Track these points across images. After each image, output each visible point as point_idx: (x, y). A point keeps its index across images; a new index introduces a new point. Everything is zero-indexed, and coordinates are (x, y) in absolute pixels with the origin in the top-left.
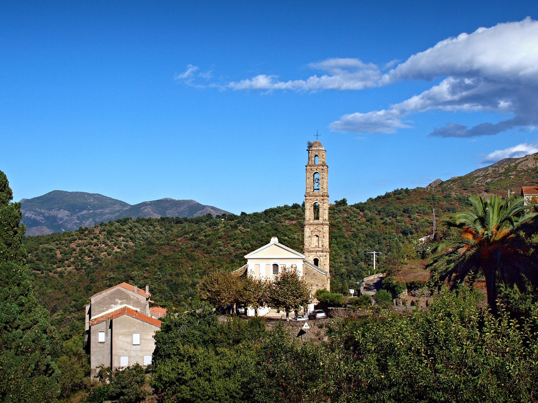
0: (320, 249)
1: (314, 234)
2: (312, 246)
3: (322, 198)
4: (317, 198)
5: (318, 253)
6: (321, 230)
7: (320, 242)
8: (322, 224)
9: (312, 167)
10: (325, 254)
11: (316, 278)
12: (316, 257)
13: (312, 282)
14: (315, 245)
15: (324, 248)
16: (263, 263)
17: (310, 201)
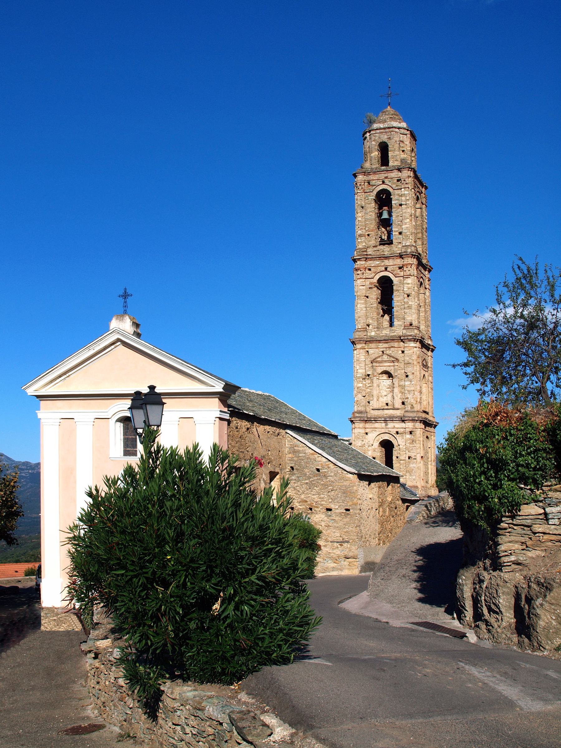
0: (398, 413)
1: (380, 370)
2: (375, 404)
3: (399, 262)
4: (387, 262)
5: (391, 425)
6: (399, 355)
7: (396, 390)
8: (401, 339)
9: (371, 177)
10: (409, 425)
11: (325, 486)
12: (387, 437)
13: (313, 497)
14: (384, 400)
15: (408, 408)
16: (83, 413)
17: (368, 274)
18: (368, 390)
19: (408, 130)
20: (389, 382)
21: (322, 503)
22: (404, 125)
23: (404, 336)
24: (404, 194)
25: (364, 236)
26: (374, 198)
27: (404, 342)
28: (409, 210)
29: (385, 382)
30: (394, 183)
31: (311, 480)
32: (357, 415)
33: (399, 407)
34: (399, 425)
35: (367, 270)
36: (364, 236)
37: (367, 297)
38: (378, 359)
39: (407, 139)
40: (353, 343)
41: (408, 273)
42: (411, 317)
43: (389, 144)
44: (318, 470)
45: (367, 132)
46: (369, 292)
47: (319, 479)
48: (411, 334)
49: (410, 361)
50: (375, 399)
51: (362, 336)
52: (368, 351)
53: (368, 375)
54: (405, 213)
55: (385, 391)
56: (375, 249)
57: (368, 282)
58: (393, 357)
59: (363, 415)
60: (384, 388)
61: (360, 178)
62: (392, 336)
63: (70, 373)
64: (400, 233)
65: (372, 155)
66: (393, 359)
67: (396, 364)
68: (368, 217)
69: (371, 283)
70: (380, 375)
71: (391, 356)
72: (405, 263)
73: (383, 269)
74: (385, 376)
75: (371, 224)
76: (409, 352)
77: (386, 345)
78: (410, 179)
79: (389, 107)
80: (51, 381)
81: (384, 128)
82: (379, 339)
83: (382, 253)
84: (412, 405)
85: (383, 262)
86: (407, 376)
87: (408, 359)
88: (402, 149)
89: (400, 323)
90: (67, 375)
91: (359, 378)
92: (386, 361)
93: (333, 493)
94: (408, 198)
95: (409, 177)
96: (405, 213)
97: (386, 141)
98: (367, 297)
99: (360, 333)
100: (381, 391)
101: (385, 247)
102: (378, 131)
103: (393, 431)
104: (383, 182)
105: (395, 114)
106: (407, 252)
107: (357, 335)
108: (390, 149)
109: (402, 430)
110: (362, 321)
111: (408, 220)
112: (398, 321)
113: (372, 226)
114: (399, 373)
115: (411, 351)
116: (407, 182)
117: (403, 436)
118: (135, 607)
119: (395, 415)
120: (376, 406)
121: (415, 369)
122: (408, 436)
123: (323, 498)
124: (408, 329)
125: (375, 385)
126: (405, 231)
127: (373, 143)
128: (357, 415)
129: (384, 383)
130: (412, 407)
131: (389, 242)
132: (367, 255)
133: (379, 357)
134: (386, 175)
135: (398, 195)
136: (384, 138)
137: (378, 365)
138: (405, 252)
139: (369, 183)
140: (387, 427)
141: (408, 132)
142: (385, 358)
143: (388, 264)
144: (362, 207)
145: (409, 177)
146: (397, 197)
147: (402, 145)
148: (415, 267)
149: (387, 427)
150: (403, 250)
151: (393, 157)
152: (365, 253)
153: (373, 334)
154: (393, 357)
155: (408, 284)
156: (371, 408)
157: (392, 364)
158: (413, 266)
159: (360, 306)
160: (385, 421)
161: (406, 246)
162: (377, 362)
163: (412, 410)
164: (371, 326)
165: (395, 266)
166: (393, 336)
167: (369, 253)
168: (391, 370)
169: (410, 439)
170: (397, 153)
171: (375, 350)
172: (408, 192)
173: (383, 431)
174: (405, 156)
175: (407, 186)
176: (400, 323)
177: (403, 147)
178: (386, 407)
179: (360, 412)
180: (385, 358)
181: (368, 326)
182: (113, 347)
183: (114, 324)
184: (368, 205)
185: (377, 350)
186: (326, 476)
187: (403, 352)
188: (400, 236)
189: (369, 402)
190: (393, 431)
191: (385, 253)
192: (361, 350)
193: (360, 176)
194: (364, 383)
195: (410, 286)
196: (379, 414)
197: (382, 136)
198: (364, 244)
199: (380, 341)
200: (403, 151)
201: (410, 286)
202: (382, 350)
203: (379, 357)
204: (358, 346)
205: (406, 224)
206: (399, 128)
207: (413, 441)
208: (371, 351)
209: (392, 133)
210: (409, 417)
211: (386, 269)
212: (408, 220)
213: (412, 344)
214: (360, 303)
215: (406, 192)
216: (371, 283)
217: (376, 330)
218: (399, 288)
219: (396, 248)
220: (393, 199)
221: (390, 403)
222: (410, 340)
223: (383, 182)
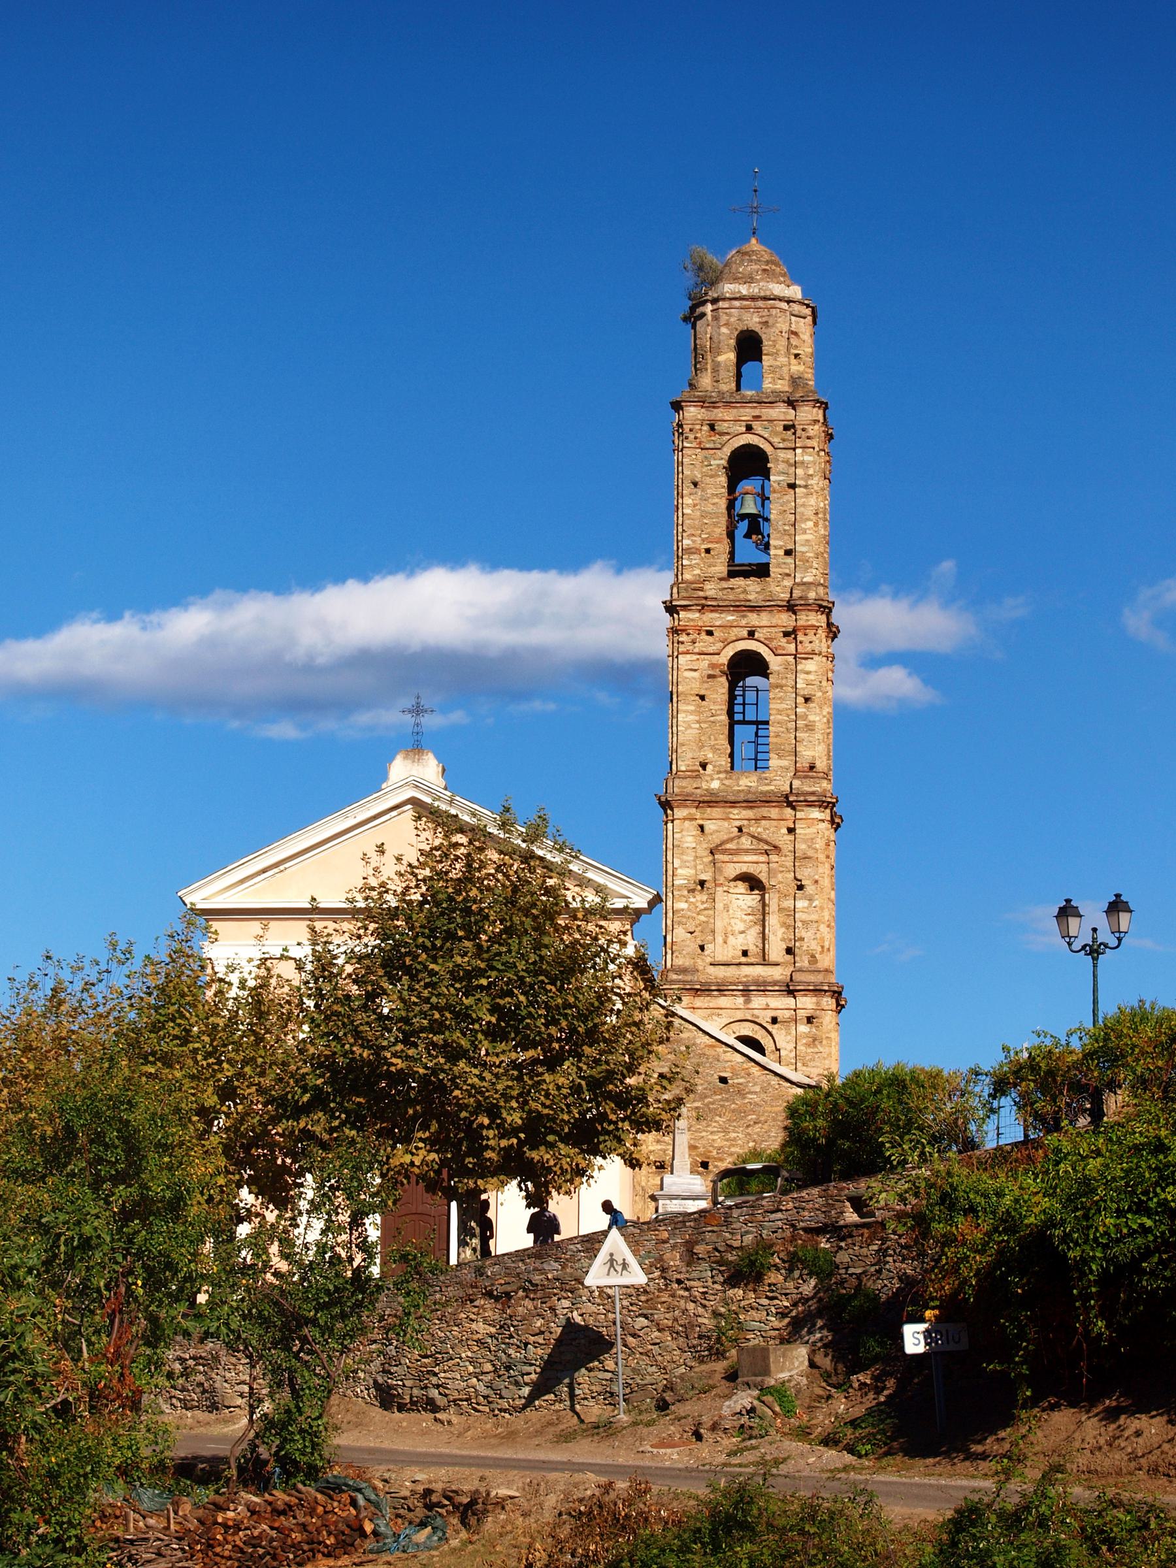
1: (732, 870)
3: (785, 620)
4: (753, 619)
5: (758, 1001)
7: (773, 920)
8: (788, 801)
9: (719, 413)
10: (807, 1003)
11: (741, 1113)
14: (739, 942)
15: (803, 962)
18: (702, 918)
19: (808, 306)
20: (752, 899)
21: (733, 1149)
22: (796, 292)
23: (797, 795)
24: (802, 463)
25: (696, 551)
26: (724, 463)
27: (794, 808)
28: (812, 501)
29: (743, 900)
30: (776, 434)
31: (706, 1101)
32: (675, 977)
33: (780, 960)
34: (781, 1003)
35: (703, 634)
36: (696, 551)
37: (702, 698)
38: (728, 846)
39: (804, 327)
40: (666, 805)
41: (809, 648)
42: (815, 750)
43: (763, 337)
44: (723, 1080)
45: (707, 301)
46: (706, 685)
47: (727, 1100)
48: (813, 789)
49: (810, 853)
50: (719, 939)
51: (689, 790)
52: (702, 827)
53: (702, 883)
54: (803, 505)
55: (742, 920)
56: (725, 584)
57: (704, 663)
58: (767, 843)
59: (689, 978)
60: (739, 914)
61: (692, 412)
62: (764, 793)
63: (287, 865)
64: (788, 553)
65: (721, 358)
66: (766, 847)
67: (774, 858)
68: (710, 508)
69: (713, 666)
70: (732, 884)
71: (760, 840)
72: (800, 623)
73: (745, 633)
74: (741, 887)
75: (715, 525)
76: (808, 831)
77: (749, 813)
78: (816, 427)
79: (753, 241)
80: (242, 881)
81: (753, 298)
82: (732, 798)
83: (742, 596)
84: (813, 956)
85: (744, 616)
86: (800, 888)
87: (804, 846)
88: (792, 351)
89: (784, 763)
90: (282, 868)
91: (681, 887)
92: (747, 851)
93: (757, 1128)
94: (811, 472)
95: (816, 421)
96: (803, 505)
97: (757, 330)
98: (702, 698)
99: (684, 783)
100: (733, 921)
101: (749, 582)
102: (737, 303)
103: (765, 1017)
104: (749, 428)
105: (773, 262)
106: (806, 599)
107: (680, 786)
108: (765, 350)
109: (788, 1014)
110: (690, 755)
111: (810, 524)
112: (780, 757)
113: (718, 531)
114: (780, 880)
115: (813, 830)
116: (811, 433)
117: (788, 1029)
118: (791, 1205)
119: (769, 979)
120: (720, 958)
121: (821, 870)
122: (803, 1028)
123: (734, 1139)
124: (806, 777)
125: (719, 906)
126: (804, 549)
127: (724, 330)
128: (675, 977)
129: (740, 903)
130: (813, 959)
131: (761, 571)
132: (706, 598)
133: (732, 839)
134: (757, 412)
135: (787, 462)
136: (753, 321)
137: (726, 858)
138: (801, 598)
139: (712, 427)
140: (751, 1006)
141: (808, 311)
142: (746, 842)
143: (757, 624)
144: (695, 484)
145: (816, 421)
146: (782, 467)
147: (794, 341)
148: (824, 635)
149: (751, 1006)
150: (796, 594)
151: (773, 369)
152: (701, 594)
153: (715, 785)
154: (767, 843)
155: (808, 673)
156: (709, 960)
157: (763, 858)
158: (820, 631)
159: (687, 717)
160: (746, 992)
161: (804, 584)
162: (725, 852)
163: (813, 968)
164: (709, 767)
165: (773, 630)
166: (768, 792)
167: (710, 593)
168: (762, 874)
169: (807, 1035)
170: (782, 360)
171: (720, 823)
172: (811, 459)
173: (739, 1015)
174: (801, 368)
175: (809, 443)
176: (784, 763)
177: (796, 347)
178: (743, 960)
179: (684, 970)
180: (746, 842)
181: (704, 766)
182: (394, 813)
183: (400, 769)
184: (708, 480)
185: (726, 824)
186: (741, 1093)
187: (791, 831)
188: (790, 560)
189: (702, 948)
190: (765, 1017)
191: (750, 597)
192: (687, 823)
193: (692, 409)
194: (692, 900)
195: (811, 677)
196: (728, 974)
197: (746, 316)
198: (697, 572)
199: (733, 804)
200: (796, 356)
201: (811, 677)
202: (738, 823)
203: (732, 839)
204: (679, 813)
205: (805, 533)
206: (789, 302)
207: (814, 1040)
208: (710, 826)
209: (774, 312)
210: (809, 984)
211: (751, 634)
212: (810, 524)
213: (816, 813)
214: (685, 711)
215: (807, 458)
216: (713, 666)
217: (722, 776)
218: (784, 682)
219: (778, 588)
220: (772, 471)
221: (752, 949)
222: (810, 804)
223: (749, 428)
